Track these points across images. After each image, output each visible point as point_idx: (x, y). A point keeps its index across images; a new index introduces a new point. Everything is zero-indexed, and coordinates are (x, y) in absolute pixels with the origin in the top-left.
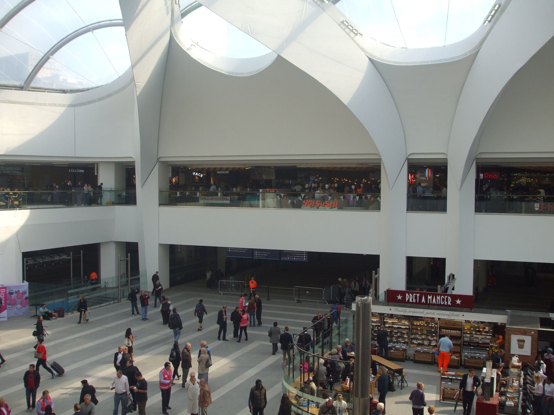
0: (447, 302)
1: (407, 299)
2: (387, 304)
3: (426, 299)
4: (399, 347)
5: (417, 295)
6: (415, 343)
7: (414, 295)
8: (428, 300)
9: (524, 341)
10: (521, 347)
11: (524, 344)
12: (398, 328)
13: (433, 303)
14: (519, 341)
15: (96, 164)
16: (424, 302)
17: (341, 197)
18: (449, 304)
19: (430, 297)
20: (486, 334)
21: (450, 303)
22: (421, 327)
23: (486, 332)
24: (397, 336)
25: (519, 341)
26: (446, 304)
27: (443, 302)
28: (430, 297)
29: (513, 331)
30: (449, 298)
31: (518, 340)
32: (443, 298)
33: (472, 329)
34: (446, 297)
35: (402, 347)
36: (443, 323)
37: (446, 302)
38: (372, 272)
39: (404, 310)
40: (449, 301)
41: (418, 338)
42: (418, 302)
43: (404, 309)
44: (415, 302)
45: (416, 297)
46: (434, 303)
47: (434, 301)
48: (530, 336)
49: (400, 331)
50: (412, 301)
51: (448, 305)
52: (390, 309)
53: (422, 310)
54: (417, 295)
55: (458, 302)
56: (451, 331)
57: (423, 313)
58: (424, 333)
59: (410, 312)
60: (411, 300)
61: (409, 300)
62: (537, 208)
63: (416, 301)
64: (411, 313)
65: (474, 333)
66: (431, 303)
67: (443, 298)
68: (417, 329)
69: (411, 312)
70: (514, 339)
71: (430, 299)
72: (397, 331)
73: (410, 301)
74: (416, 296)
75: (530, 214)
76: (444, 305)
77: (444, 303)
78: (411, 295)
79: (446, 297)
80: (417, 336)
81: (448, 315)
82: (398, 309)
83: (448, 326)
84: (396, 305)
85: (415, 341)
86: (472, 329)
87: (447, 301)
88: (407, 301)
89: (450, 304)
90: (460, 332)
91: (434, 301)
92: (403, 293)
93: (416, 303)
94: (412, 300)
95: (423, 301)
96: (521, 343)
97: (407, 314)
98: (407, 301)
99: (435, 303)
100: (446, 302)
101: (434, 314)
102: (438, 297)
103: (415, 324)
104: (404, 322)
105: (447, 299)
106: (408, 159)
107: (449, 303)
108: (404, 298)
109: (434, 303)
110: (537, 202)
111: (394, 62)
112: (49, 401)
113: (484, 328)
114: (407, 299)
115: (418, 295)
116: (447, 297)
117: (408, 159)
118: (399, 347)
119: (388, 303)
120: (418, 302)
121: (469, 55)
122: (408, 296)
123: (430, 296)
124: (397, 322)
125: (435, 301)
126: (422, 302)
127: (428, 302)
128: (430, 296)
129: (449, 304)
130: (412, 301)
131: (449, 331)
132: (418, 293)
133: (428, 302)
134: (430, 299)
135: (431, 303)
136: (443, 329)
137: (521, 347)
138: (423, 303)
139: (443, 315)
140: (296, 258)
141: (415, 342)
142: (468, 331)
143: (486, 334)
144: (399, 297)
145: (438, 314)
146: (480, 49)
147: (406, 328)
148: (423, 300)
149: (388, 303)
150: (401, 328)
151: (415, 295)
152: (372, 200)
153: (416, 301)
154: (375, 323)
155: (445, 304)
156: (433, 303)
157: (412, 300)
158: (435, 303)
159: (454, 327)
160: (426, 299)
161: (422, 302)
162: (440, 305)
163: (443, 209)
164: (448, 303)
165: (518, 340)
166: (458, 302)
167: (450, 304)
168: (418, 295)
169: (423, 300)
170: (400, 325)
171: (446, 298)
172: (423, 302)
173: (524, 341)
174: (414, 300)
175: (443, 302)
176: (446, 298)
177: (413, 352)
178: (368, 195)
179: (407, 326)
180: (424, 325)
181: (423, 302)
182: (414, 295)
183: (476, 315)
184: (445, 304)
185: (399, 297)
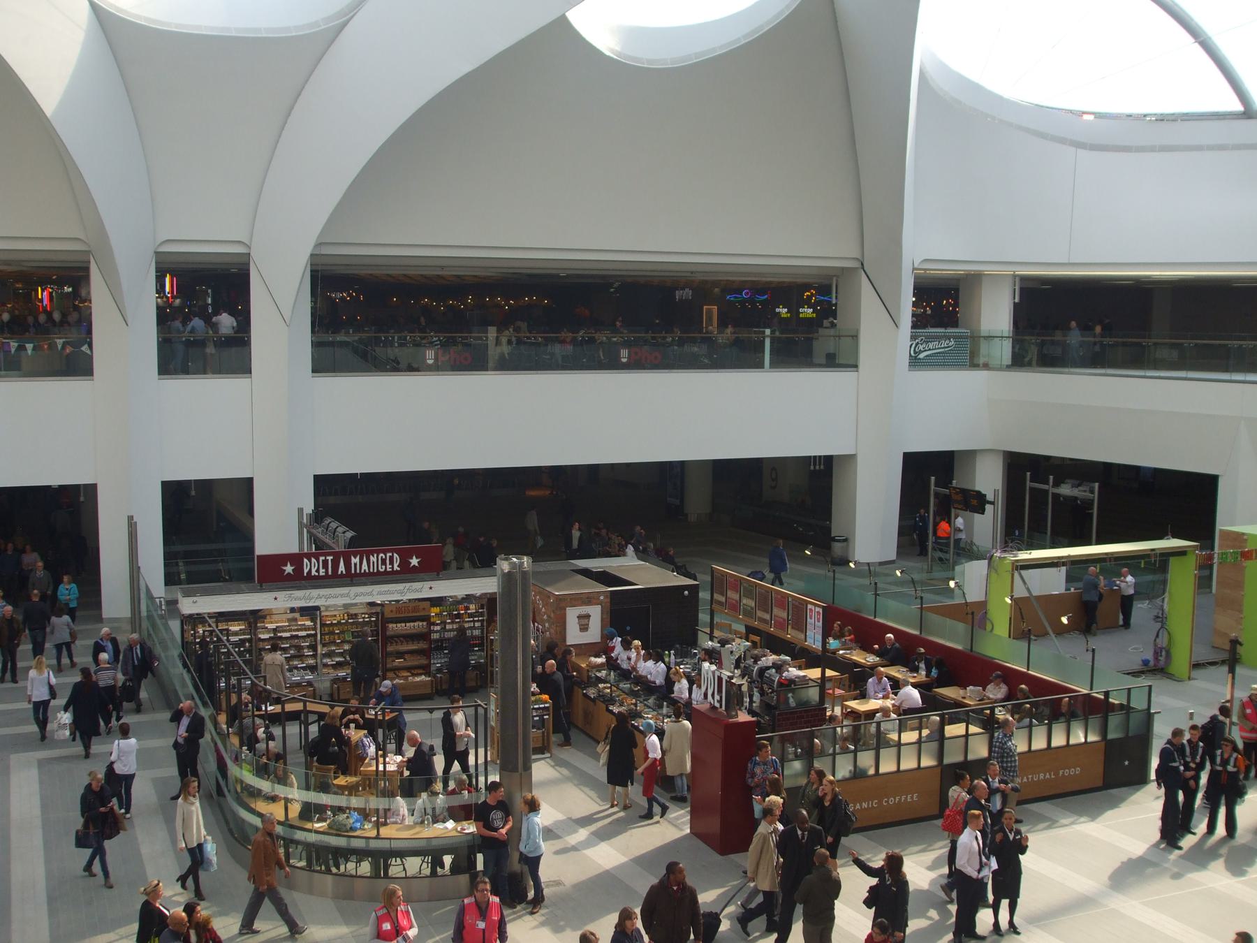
0: (391, 566)
1: (306, 571)
2: (259, 587)
3: (348, 565)
4: (299, 678)
5: (328, 558)
6: (329, 663)
7: (322, 558)
8: (351, 567)
9: (588, 616)
10: (584, 628)
11: (589, 621)
12: (293, 637)
13: (363, 571)
14: (579, 617)
15: (834, 279)
16: (344, 572)
17: (27, 345)
18: (395, 569)
19: (355, 560)
20: (472, 619)
21: (398, 566)
22: (341, 628)
23: (471, 615)
24: (289, 655)
25: (579, 617)
26: (391, 570)
27: (384, 567)
28: (355, 560)
29: (569, 600)
30: (395, 555)
31: (578, 617)
32: (384, 557)
33: (444, 613)
34: (389, 555)
35: (306, 678)
36: (392, 611)
37: (389, 566)
38: (930, 478)
39: (307, 595)
40: (395, 562)
41: (337, 651)
42: (330, 573)
43: (307, 592)
44: (324, 574)
45: (325, 563)
46: (365, 571)
47: (365, 567)
48: (598, 604)
49: (294, 644)
50: (317, 574)
51: (393, 572)
52: (276, 599)
53: (400, 586)
54: (328, 558)
55: (414, 561)
56: (408, 624)
57: (348, 595)
58: (347, 639)
59: (319, 597)
60: (314, 573)
61: (310, 570)
62: (432, 359)
63: (327, 572)
64: (323, 599)
65: (449, 621)
66: (358, 571)
67: (384, 557)
68: (333, 633)
69: (321, 598)
70: (572, 614)
71: (355, 565)
72: (288, 645)
73: (313, 574)
74: (325, 562)
75: (789, 370)
76: (386, 572)
77: (386, 568)
78: (313, 560)
79: (389, 555)
80: (333, 648)
81: (401, 592)
82: (293, 596)
83: (403, 615)
84: (381, 581)
85: (328, 660)
86: (446, 613)
87: (392, 563)
88: (305, 575)
89: (399, 569)
90: (425, 623)
91: (365, 567)
92: (296, 559)
93: (327, 576)
94: (318, 571)
95: (340, 569)
96: (584, 621)
97: (314, 602)
98: (305, 575)
99: (367, 571)
100: (388, 566)
101: (371, 594)
102: (373, 556)
103: (328, 622)
104: (303, 623)
105: (391, 558)
106: (157, 253)
107: (396, 567)
108: (298, 569)
109: (365, 571)
110: (429, 348)
111: (146, 19)
112: (972, 781)
113: (467, 608)
114: (306, 571)
115: (330, 558)
116: (391, 554)
117: (157, 253)
118: (299, 678)
119: (261, 586)
120: (330, 573)
121: (323, 27)
122: (309, 563)
123: (355, 558)
124: (287, 624)
125: (366, 566)
126: (340, 573)
127: (353, 572)
128: (355, 558)
129: (395, 569)
130: (317, 574)
131: (403, 625)
132: (329, 554)
133: (353, 572)
134: (355, 565)
135: (358, 571)
136: (392, 622)
137: (584, 628)
138: (342, 575)
139: (390, 594)
140: (820, 465)
141: (328, 661)
142: (437, 619)
143: (472, 619)
144: (289, 569)
145: (380, 593)
146: (352, 17)
147: (308, 636)
148: (342, 568)
149: (261, 586)
150: (297, 637)
151: (323, 558)
152: (68, 351)
153: (327, 572)
154: (306, 631)
155: (388, 570)
156: (363, 571)
157: (318, 571)
158: (367, 571)
159: (416, 614)
160: (348, 565)
161: (340, 573)
162: (379, 573)
163: (243, 368)
164: (393, 568)
165: (578, 617)
166: (414, 561)
167: (399, 569)
168: (330, 558)
169: (342, 568)
170: (295, 630)
171: (323, 561)
172: (342, 572)
173: (588, 616)
174: (322, 572)
175: (384, 567)
176: (390, 556)
177: (328, 684)
178: (58, 341)
179: (309, 629)
180: (347, 621)
181: (342, 572)
182: (322, 558)
183: (215, 600)
184: (388, 570)
185: (289, 569)
